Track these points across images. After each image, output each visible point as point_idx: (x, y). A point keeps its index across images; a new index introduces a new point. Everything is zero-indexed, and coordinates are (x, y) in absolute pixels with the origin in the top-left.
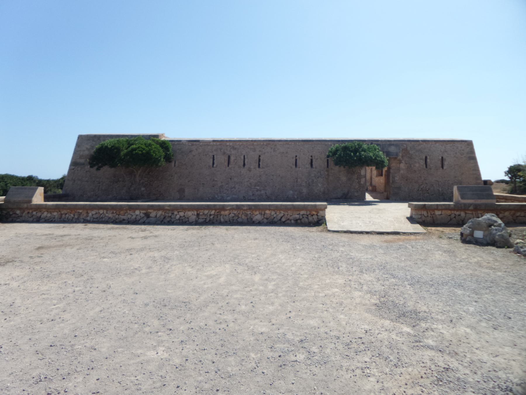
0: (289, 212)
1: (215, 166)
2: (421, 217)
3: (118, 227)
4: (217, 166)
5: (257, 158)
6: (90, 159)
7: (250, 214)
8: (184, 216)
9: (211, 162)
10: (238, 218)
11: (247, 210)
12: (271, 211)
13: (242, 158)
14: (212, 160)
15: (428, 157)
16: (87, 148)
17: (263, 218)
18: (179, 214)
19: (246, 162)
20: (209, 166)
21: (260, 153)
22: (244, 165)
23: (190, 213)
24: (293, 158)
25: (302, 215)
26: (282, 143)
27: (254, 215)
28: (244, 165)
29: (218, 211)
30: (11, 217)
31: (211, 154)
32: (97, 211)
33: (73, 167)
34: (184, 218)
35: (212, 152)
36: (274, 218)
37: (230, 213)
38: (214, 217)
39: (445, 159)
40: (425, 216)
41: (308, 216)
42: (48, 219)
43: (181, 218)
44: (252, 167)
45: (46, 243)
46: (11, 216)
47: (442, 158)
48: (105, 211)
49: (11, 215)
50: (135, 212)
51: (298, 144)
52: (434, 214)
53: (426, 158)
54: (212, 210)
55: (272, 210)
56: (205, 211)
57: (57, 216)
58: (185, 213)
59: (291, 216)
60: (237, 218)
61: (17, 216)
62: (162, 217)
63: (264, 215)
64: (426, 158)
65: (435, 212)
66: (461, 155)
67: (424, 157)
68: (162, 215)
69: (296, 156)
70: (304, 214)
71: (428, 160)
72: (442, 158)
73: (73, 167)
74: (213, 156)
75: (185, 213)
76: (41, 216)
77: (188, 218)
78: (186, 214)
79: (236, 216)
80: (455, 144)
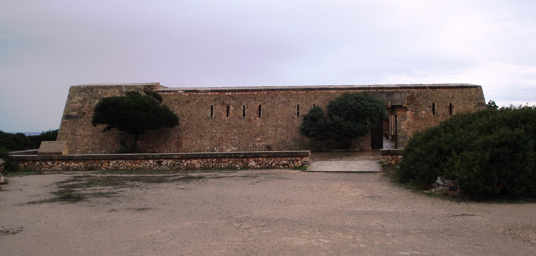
0: (278, 158)
1: (213, 116)
2: (387, 161)
3: (94, 172)
4: (215, 117)
5: (257, 108)
6: (94, 111)
7: (246, 161)
8: (191, 164)
9: (210, 113)
10: (236, 165)
11: (243, 157)
12: (263, 158)
13: (242, 108)
14: (210, 111)
15: (436, 104)
16: (79, 100)
17: (257, 164)
18: (186, 162)
19: (246, 112)
20: (208, 117)
21: (260, 103)
22: (244, 115)
23: (195, 161)
24: (295, 107)
25: (289, 161)
26: (283, 92)
27: (249, 162)
28: (244, 115)
29: (219, 159)
30: (43, 167)
31: (210, 105)
32: (117, 161)
33: (65, 121)
34: (190, 165)
35: (211, 102)
36: (266, 163)
37: (229, 161)
38: (215, 164)
39: (453, 106)
40: (390, 160)
41: (293, 161)
42: (76, 169)
43: (188, 166)
44: (252, 118)
45: (120, 192)
46: (43, 166)
47: (451, 104)
48: (124, 161)
49: (43, 166)
50: (149, 161)
51: (300, 92)
52: (397, 158)
53: (434, 104)
54: (214, 158)
55: (264, 157)
56: (208, 159)
57: (82, 166)
58: (191, 161)
59: (280, 162)
60: (235, 164)
61: (48, 166)
62: (172, 165)
63: (257, 161)
64: (434, 104)
65: (398, 156)
66: (470, 101)
67: (431, 104)
68: (172, 162)
69: (298, 105)
70: (290, 160)
71: (436, 107)
72: (451, 104)
73: (65, 121)
74: (212, 106)
75: (191, 161)
76: (69, 166)
77: (194, 165)
78: (192, 162)
79: (234, 163)
80: (463, 90)
